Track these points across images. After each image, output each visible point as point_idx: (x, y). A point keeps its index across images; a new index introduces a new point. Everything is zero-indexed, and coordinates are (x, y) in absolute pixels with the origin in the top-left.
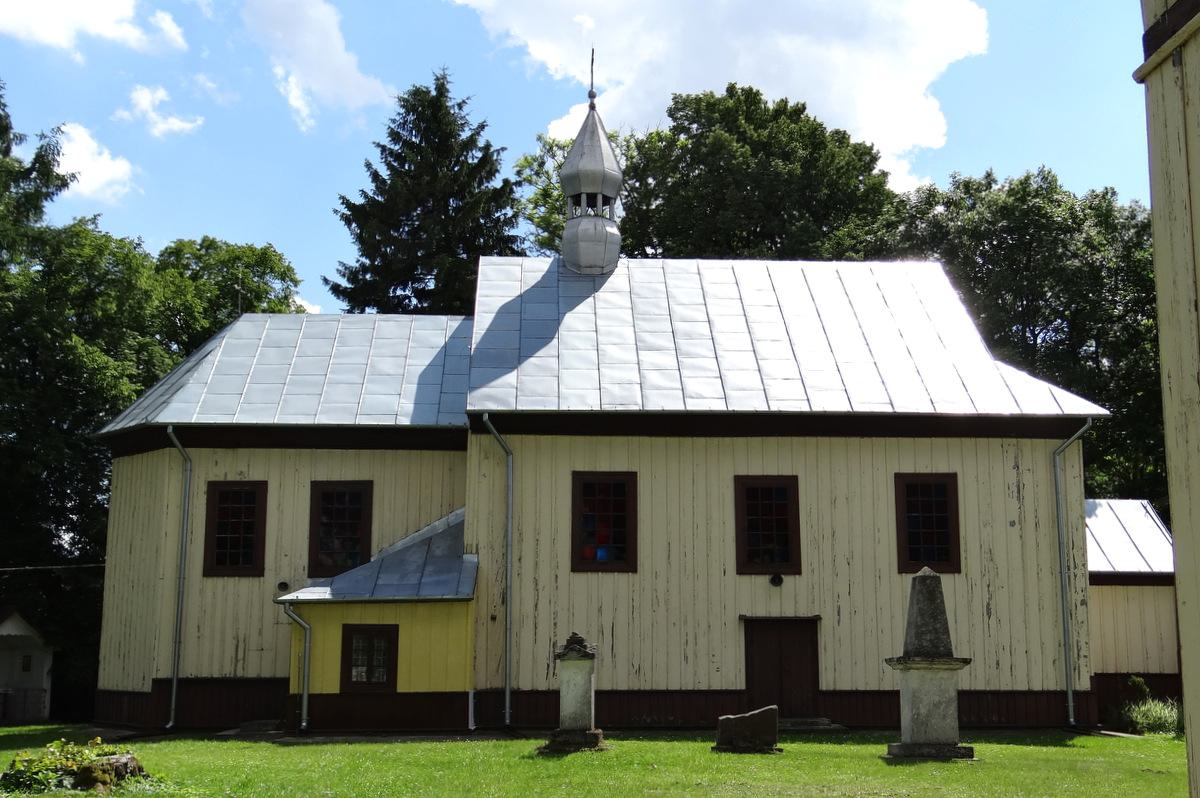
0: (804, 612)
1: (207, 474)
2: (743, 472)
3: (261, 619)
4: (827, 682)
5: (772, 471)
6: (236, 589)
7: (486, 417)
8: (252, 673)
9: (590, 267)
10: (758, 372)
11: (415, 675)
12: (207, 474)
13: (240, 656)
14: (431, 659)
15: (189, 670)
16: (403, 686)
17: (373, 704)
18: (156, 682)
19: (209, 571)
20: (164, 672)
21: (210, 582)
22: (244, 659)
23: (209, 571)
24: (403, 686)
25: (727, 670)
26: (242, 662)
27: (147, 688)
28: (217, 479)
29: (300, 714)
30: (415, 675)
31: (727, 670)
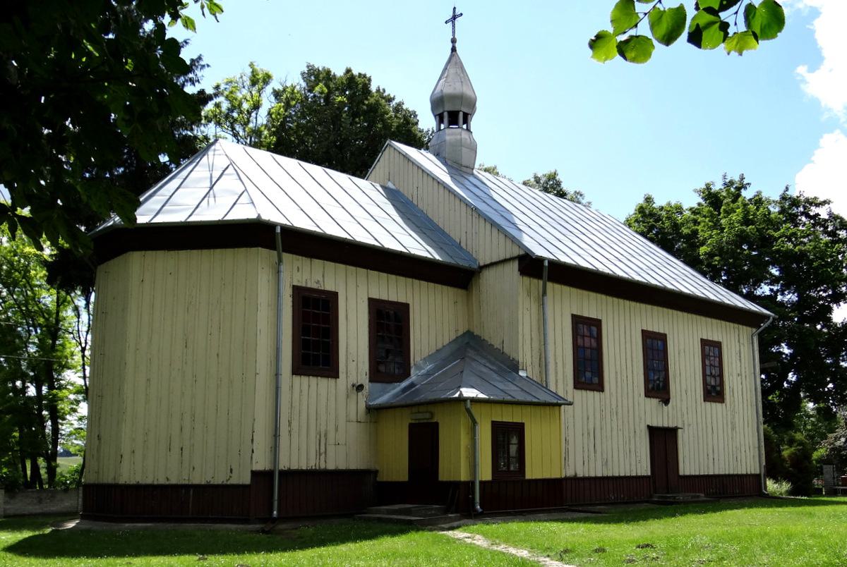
0: (671, 425)
1: (292, 278)
2: (375, 296)
3: (595, 424)
4: (681, 473)
5: (393, 298)
6: (317, 387)
7: (278, 230)
8: (331, 466)
9: (467, 167)
10: (239, 181)
11: (690, 463)
12: (292, 278)
13: (323, 450)
14: (468, 457)
15: (284, 464)
16: (528, 476)
17: (420, 494)
18: (255, 474)
19: (296, 371)
20: (262, 464)
21: (297, 379)
22: (326, 452)
23: (296, 371)
24: (528, 476)
25: (637, 462)
26: (324, 455)
27: (247, 480)
28: (299, 284)
29: (474, 498)
30: (690, 463)
31: (637, 462)
